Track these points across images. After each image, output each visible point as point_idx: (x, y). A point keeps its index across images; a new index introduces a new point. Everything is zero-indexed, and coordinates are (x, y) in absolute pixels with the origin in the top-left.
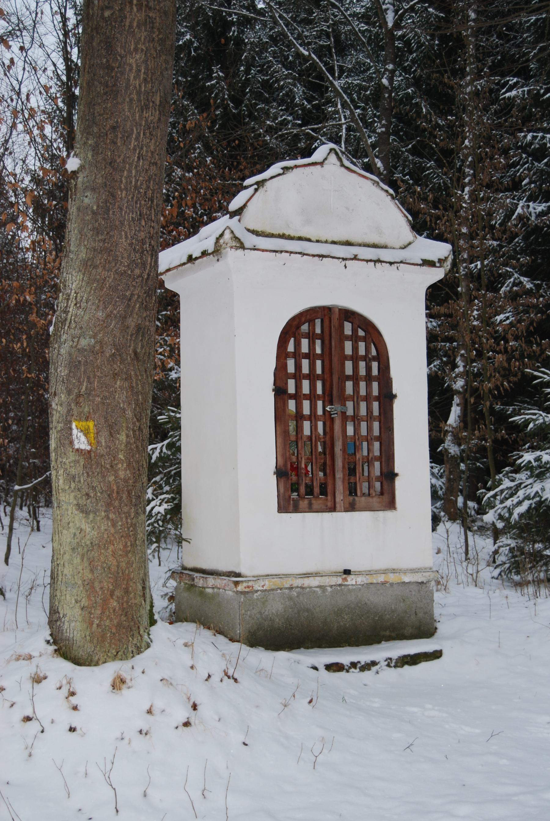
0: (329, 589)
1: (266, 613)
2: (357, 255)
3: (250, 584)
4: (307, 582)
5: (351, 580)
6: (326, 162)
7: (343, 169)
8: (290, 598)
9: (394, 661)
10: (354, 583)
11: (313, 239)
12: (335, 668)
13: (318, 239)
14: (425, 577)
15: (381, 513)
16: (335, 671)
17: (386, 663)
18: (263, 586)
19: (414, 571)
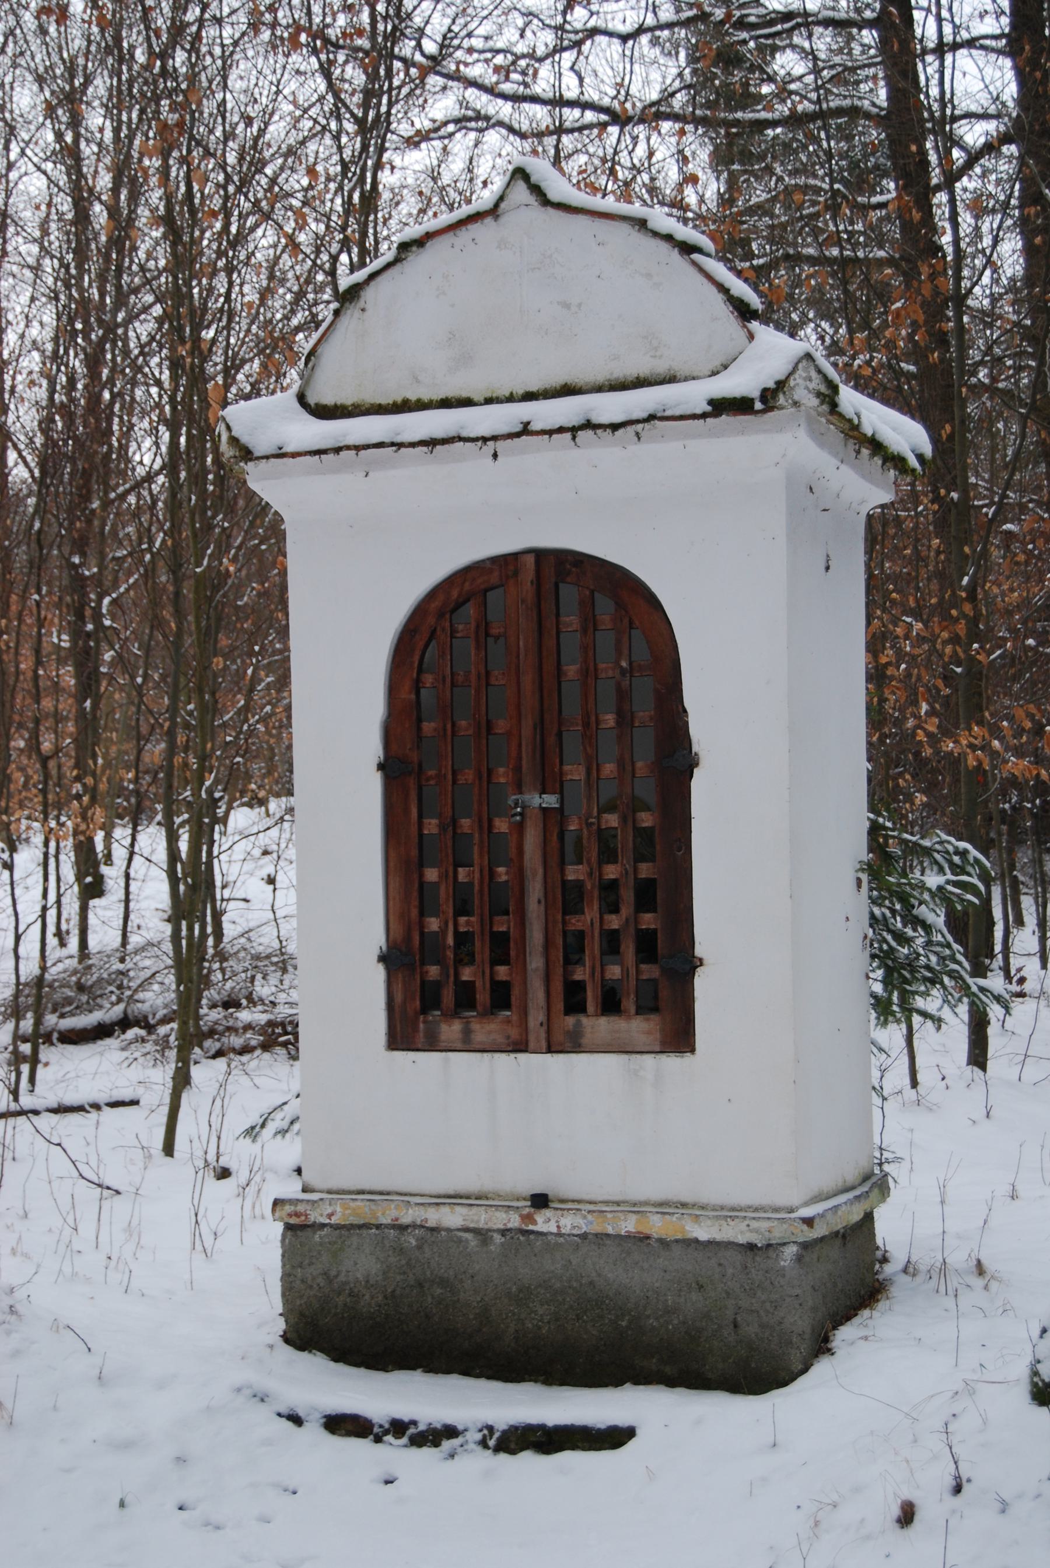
0: (498, 1238)
1: (342, 1278)
2: (528, 423)
3: (300, 1208)
4: (434, 1217)
5: (545, 1222)
6: (503, 205)
7: (550, 210)
8: (400, 1251)
9: (497, 1435)
10: (554, 1230)
11: (476, 398)
12: (350, 1427)
13: (489, 395)
14: (757, 1231)
15: (648, 1060)
16: (349, 1434)
17: (479, 1436)
18: (330, 1216)
19: (731, 1212)
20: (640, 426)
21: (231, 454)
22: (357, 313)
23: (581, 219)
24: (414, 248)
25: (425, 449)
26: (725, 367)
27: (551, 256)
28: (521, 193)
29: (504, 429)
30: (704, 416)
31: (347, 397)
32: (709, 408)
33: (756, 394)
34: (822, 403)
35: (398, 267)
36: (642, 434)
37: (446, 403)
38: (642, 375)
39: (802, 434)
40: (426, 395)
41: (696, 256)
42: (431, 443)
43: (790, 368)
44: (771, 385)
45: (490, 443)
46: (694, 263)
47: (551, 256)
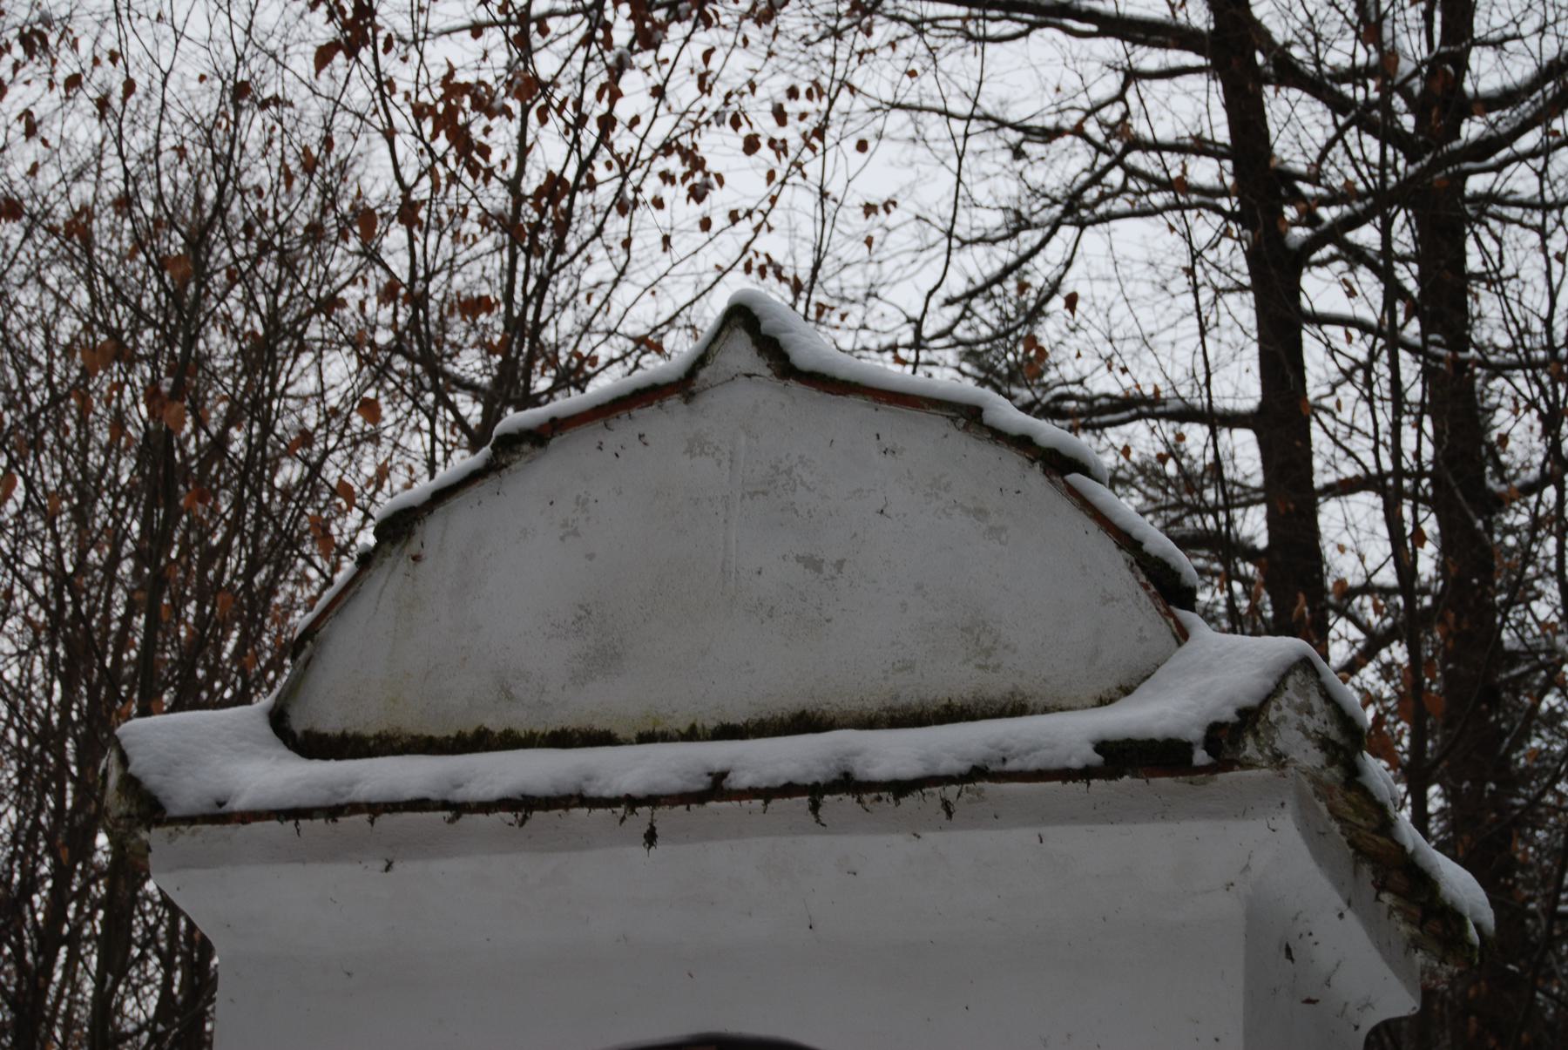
2: (723, 775)
7: (795, 387)
20: (951, 791)
21: (122, 809)
22: (404, 565)
23: (854, 406)
24: (526, 447)
25: (509, 816)
26: (1127, 691)
27: (789, 472)
28: (741, 353)
29: (675, 784)
30: (1085, 774)
31: (368, 723)
32: (1097, 759)
33: (1196, 734)
34: (1331, 762)
35: (490, 483)
36: (958, 808)
37: (561, 739)
38: (957, 702)
39: (1287, 824)
40: (521, 722)
41: (1075, 478)
42: (523, 805)
43: (1270, 683)
44: (1229, 715)
45: (644, 811)
46: (1073, 492)
47: (789, 472)
